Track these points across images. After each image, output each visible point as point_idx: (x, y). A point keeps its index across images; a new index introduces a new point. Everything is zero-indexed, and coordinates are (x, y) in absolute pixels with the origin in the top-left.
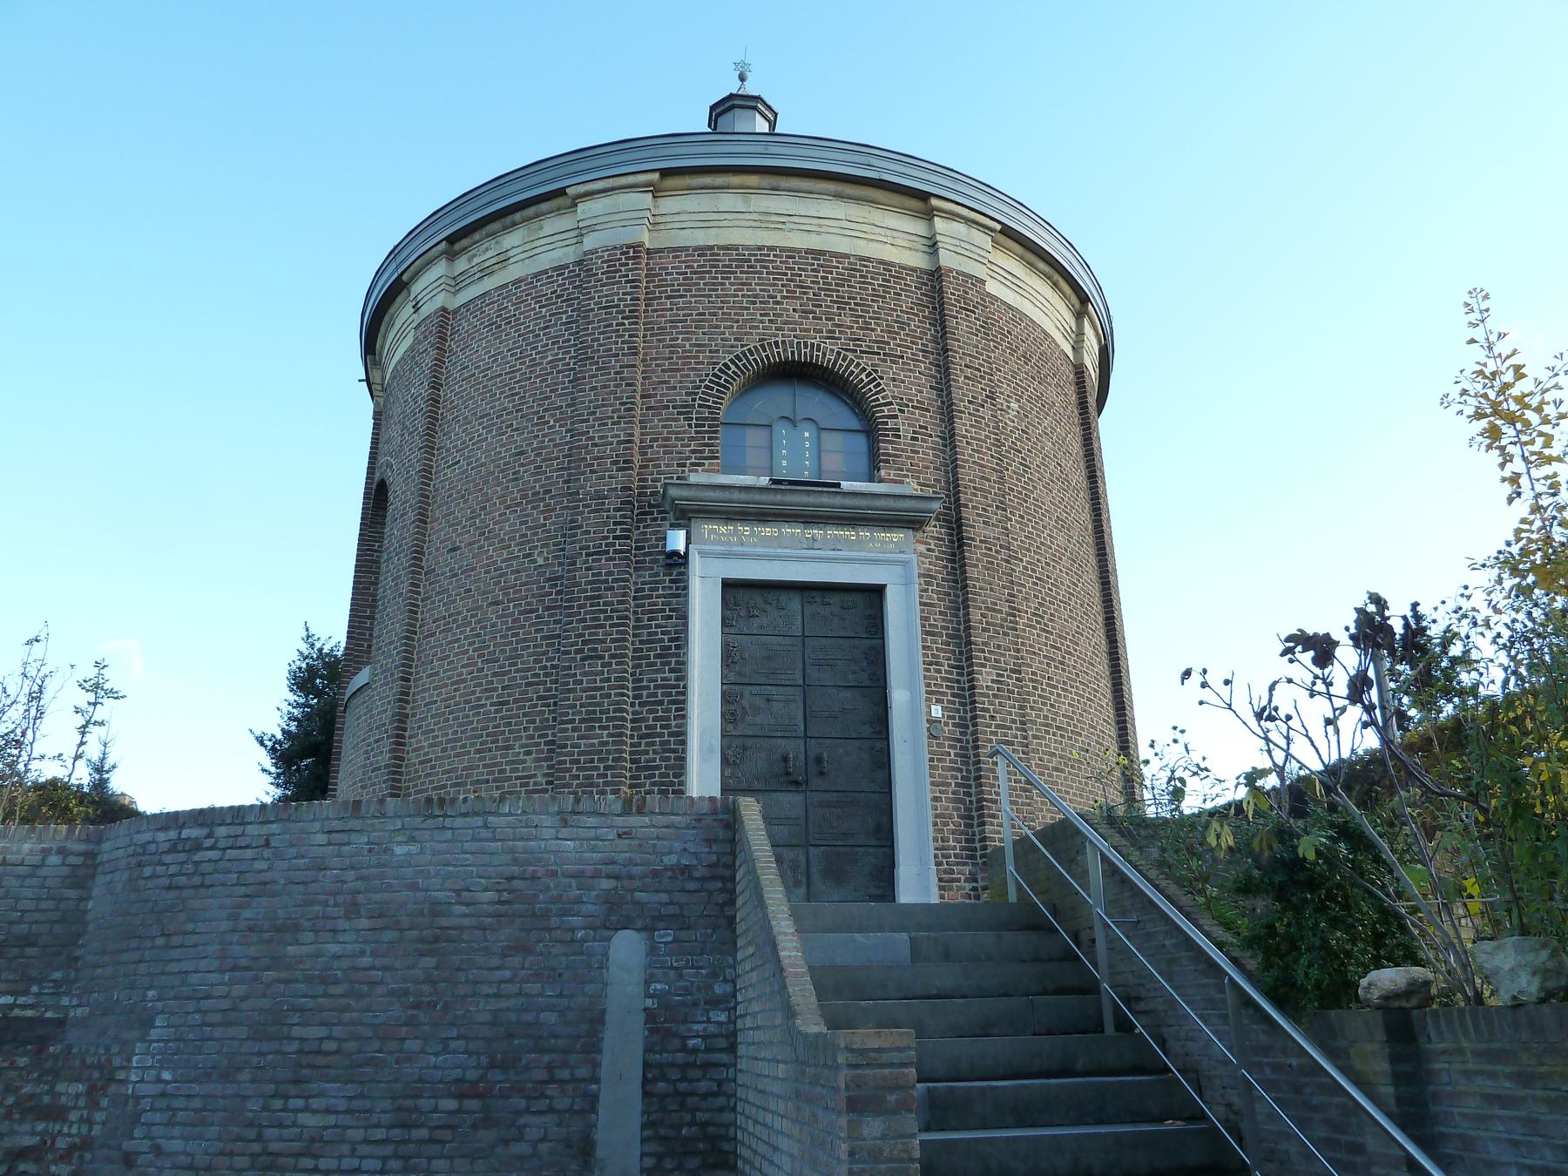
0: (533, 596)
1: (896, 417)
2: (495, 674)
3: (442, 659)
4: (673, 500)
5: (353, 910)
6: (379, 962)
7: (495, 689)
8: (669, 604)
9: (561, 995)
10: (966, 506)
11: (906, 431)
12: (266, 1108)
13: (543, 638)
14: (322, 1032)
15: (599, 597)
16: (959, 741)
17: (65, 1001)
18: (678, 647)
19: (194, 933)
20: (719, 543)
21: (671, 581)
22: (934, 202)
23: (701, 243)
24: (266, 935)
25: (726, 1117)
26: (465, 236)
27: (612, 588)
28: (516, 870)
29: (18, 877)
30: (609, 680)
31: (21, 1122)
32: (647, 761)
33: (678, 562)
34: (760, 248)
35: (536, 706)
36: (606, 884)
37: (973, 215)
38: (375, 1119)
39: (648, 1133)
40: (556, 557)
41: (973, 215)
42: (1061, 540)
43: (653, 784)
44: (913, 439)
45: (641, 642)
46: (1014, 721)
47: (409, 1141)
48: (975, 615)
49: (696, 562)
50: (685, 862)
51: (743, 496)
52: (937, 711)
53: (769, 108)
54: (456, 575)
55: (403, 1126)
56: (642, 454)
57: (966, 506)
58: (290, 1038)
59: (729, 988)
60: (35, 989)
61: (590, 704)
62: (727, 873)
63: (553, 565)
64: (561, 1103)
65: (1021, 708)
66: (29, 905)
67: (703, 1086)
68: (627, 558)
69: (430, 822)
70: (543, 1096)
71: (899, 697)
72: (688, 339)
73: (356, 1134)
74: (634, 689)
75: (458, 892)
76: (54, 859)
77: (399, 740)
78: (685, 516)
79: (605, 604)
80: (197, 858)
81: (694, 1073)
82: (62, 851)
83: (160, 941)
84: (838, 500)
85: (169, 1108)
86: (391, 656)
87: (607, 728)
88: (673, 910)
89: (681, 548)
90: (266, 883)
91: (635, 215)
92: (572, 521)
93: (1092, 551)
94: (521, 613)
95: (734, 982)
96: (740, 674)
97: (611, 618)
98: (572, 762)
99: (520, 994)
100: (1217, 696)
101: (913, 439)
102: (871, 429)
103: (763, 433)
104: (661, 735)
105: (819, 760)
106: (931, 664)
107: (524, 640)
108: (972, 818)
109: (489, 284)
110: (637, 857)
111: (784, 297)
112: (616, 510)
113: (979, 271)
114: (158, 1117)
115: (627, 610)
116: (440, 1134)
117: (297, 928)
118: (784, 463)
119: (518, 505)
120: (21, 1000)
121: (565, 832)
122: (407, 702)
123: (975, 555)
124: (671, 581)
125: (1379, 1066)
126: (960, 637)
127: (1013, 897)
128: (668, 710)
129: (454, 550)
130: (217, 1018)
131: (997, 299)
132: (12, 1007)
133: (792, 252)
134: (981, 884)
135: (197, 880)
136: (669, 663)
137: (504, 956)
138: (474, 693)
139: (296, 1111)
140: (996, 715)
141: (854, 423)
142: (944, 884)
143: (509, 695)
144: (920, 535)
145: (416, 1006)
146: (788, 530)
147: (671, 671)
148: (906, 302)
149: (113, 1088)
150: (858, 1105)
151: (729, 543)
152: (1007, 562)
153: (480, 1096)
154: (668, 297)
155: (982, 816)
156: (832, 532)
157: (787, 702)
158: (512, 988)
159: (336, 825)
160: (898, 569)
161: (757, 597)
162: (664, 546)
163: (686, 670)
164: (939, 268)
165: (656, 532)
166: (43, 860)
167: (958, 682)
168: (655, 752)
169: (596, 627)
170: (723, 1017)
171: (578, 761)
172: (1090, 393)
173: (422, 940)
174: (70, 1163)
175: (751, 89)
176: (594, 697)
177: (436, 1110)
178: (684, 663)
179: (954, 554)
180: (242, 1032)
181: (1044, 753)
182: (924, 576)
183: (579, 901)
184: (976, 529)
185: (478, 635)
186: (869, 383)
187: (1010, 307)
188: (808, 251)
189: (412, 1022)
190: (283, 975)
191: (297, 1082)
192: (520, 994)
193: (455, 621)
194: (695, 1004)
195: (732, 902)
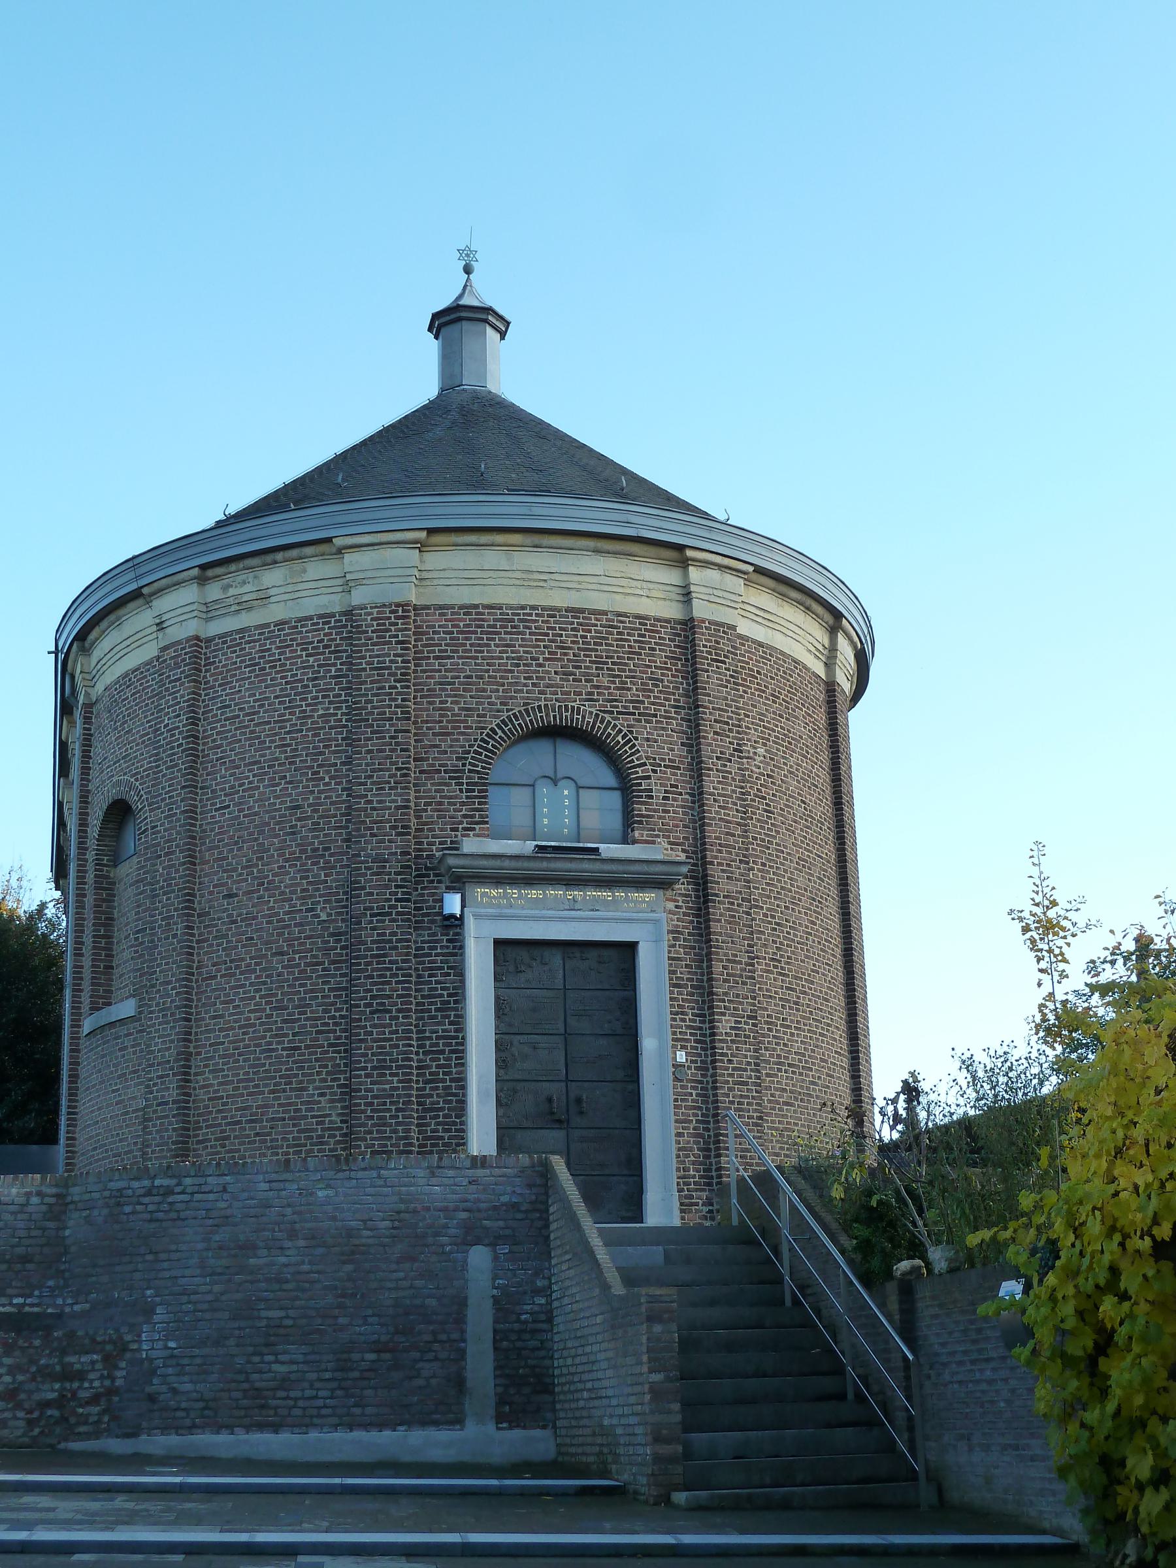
0: (319, 949)
1: (649, 777)
4: (451, 868)
5: (293, 1235)
6: (315, 1268)
7: (286, 1035)
9: (438, 1288)
10: (712, 863)
11: (658, 792)
12: (249, 1362)
14: (282, 1313)
16: (701, 1082)
17: (60, 1301)
18: (456, 1002)
19: (177, 1251)
20: (491, 906)
23: (467, 601)
24: (233, 1252)
25: (547, 1362)
27: (396, 948)
28: (403, 1206)
29: (12, 1213)
30: (397, 1032)
31: (43, 1383)
32: (432, 1103)
33: (454, 924)
34: (523, 608)
35: (327, 1052)
36: (464, 1215)
37: (727, 561)
38: (323, 1366)
39: (498, 1372)
41: (727, 561)
42: (801, 881)
43: (438, 1124)
44: (665, 798)
45: (423, 997)
46: (749, 1063)
47: (348, 1379)
48: (717, 967)
49: (471, 925)
50: (514, 1200)
51: (514, 864)
52: (681, 1057)
53: (501, 318)
55: (342, 1370)
56: (419, 817)
57: (712, 863)
58: (260, 1318)
59: (546, 1282)
60: (36, 1293)
61: (381, 1054)
62: (542, 1207)
63: (336, 921)
64: (443, 1355)
65: (756, 1051)
66: (22, 1233)
67: (532, 1343)
68: (409, 920)
69: (340, 1175)
70: (430, 1350)
71: (649, 1044)
72: (457, 703)
73: (314, 1376)
74: (418, 1039)
75: (364, 1221)
76: (35, 1200)
77: (185, 1077)
78: (459, 882)
79: (390, 962)
80: (170, 1199)
81: (527, 1336)
82: (39, 1194)
83: (149, 1257)
84: (598, 866)
85: (178, 1365)
86: (169, 996)
87: (397, 1075)
88: (508, 1232)
89: (458, 912)
90: (227, 1217)
93: (834, 883)
95: (550, 1279)
96: (510, 1025)
97: (396, 975)
98: (366, 1104)
99: (411, 1287)
100: (947, 1015)
101: (665, 798)
102: (627, 788)
103: (527, 791)
104: (443, 1081)
105: (579, 1101)
106: (677, 1013)
107: (312, 991)
108: (709, 1150)
110: (482, 1197)
111: (545, 659)
114: (170, 1371)
115: (410, 968)
116: (367, 1374)
117: (254, 1247)
118: (546, 821)
120: (29, 1301)
121: (434, 1181)
122: (190, 1041)
123: (719, 910)
125: (894, 1305)
126: (702, 987)
127: (735, 1222)
128: (450, 1059)
129: (230, 896)
130: (205, 1306)
132: (24, 1305)
133: (553, 611)
134: (716, 1207)
135: (173, 1215)
136: (448, 1017)
137: (398, 1263)
138: (264, 1037)
139: (269, 1363)
140: (734, 1057)
141: (610, 780)
142: (685, 1207)
143: (301, 1041)
144: (669, 893)
145: (343, 1296)
148: (660, 657)
149: (128, 1355)
150: (651, 1319)
151: (499, 906)
152: (748, 914)
153: (389, 1351)
155: (718, 1149)
156: (592, 893)
158: (405, 1284)
159: (274, 1176)
160: (650, 927)
161: (523, 954)
162: (442, 907)
163: (464, 1023)
164: (692, 619)
165: (433, 894)
166: (28, 1200)
167: (700, 1029)
170: (543, 1301)
171: (372, 1104)
172: (834, 707)
173: (342, 1254)
174: (99, 1405)
176: (384, 1047)
177: (363, 1360)
178: (461, 1016)
179: (699, 909)
180: (226, 1315)
181: (776, 1089)
183: (446, 1227)
184: (721, 885)
185: (265, 983)
186: (625, 744)
187: (761, 644)
189: (340, 1306)
190: (249, 1278)
191: (267, 1345)
192: (411, 1287)
193: (237, 967)
194: (525, 1293)
195: (547, 1226)
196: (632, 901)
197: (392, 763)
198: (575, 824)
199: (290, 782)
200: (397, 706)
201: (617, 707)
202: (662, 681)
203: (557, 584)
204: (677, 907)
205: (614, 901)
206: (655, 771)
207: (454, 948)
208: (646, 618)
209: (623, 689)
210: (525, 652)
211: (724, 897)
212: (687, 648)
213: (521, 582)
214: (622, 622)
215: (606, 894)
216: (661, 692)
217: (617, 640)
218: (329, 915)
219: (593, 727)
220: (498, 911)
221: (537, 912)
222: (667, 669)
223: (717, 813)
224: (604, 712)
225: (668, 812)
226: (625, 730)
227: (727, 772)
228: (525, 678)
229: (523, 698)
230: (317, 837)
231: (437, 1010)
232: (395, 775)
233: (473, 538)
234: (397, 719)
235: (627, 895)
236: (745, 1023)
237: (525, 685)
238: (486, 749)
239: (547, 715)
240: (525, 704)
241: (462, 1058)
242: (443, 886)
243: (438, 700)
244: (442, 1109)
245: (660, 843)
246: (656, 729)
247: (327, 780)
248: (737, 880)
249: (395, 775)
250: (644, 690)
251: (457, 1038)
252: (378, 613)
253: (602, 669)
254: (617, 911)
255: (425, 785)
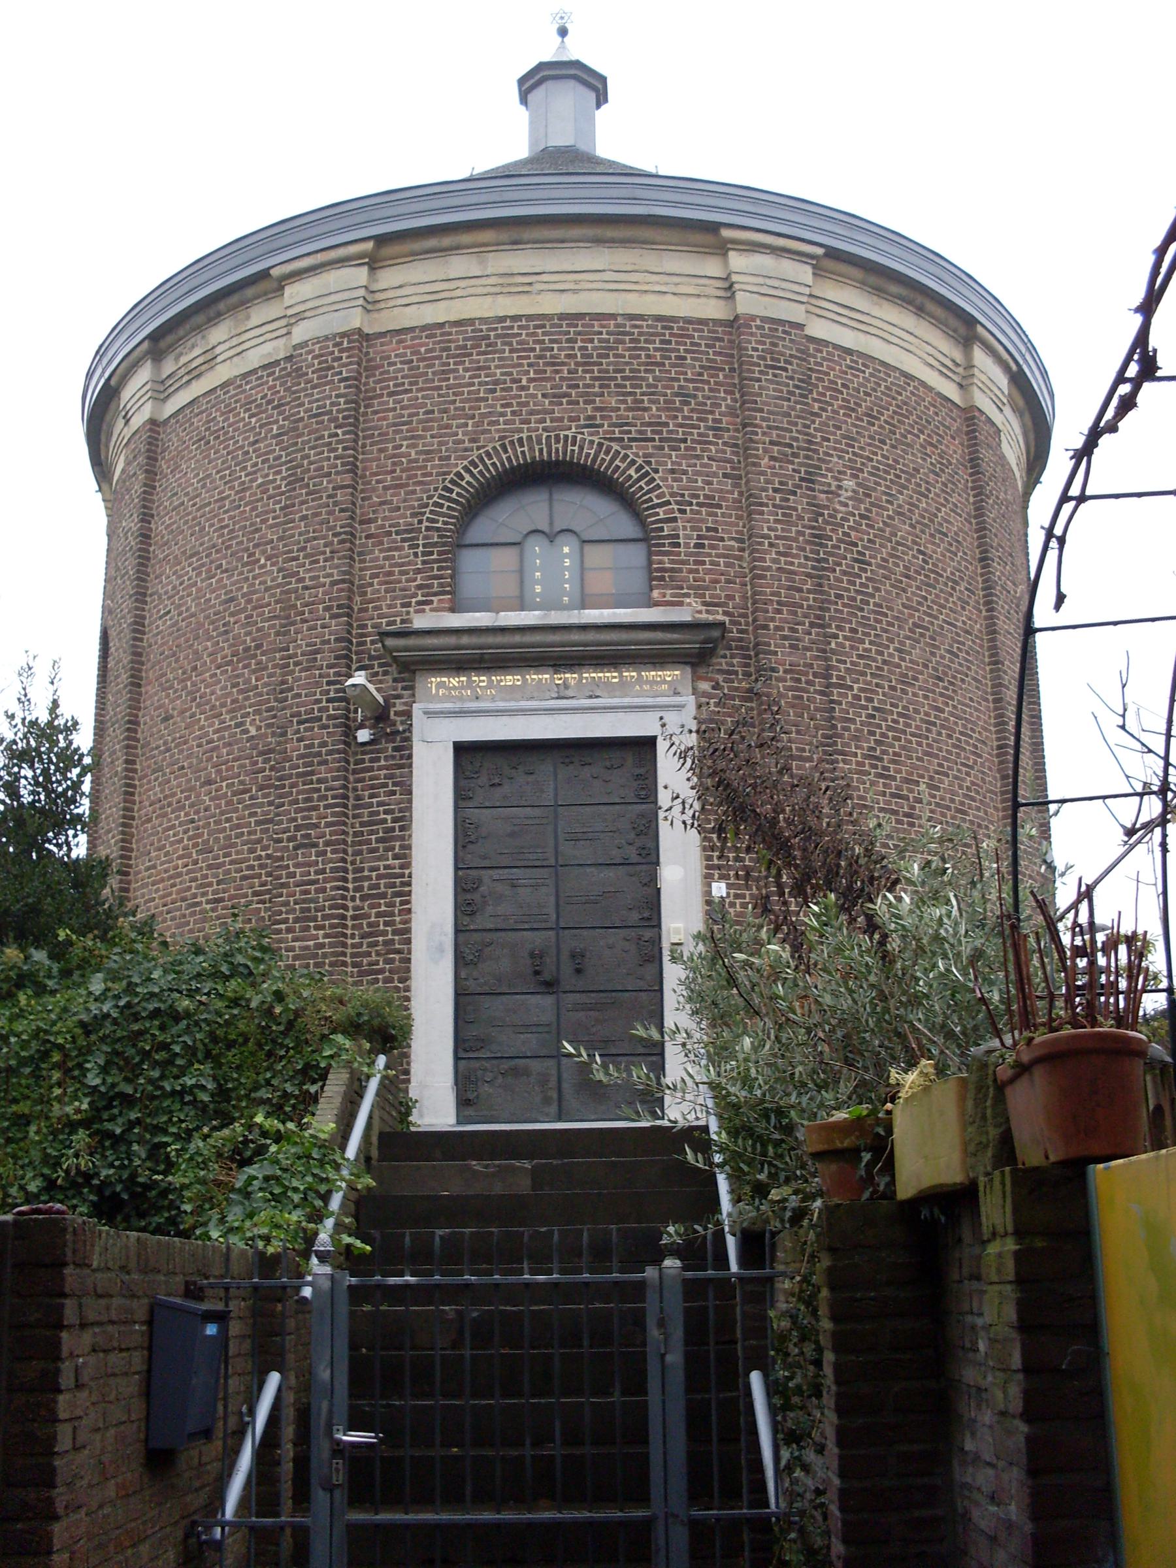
1: (675, 520)
2: (210, 867)
7: (210, 885)
13: (258, 823)
18: (402, 829)
20: (449, 698)
21: (395, 749)
22: (726, 233)
23: (430, 320)
30: (323, 871)
32: (370, 964)
34: (502, 319)
37: (782, 242)
40: (268, 726)
41: (782, 242)
45: (362, 824)
54: (168, 750)
61: (304, 901)
72: (414, 446)
79: (319, 781)
87: (322, 927)
91: (346, 295)
92: (283, 682)
94: (234, 794)
97: (325, 798)
101: (697, 546)
103: (512, 552)
104: (385, 933)
107: (238, 826)
111: (530, 380)
112: (330, 667)
113: (796, 313)
118: (538, 589)
119: (230, 663)
129: (166, 719)
131: (826, 343)
141: (625, 526)
147: (396, 857)
151: (461, 698)
154: (391, 394)
156: (589, 675)
157: (535, 886)
168: (378, 954)
175: (577, 50)
178: (409, 847)
185: (192, 821)
187: (849, 351)
188: (562, 317)
193: (170, 805)
196: (647, 682)
199: (226, 571)
200: (336, 458)
202: (695, 397)
203: (545, 287)
205: (623, 683)
206: (683, 512)
207: (402, 757)
209: (639, 409)
210: (502, 374)
211: (786, 671)
212: (732, 356)
213: (497, 289)
214: (636, 326)
215: (611, 676)
217: (630, 349)
218: (259, 728)
219: (594, 460)
222: (702, 381)
223: (774, 561)
224: (611, 440)
225: (704, 563)
226: (640, 461)
227: (789, 508)
228: (503, 406)
229: (498, 431)
231: (378, 841)
232: (332, 543)
233: (432, 243)
235: (639, 675)
237: (503, 415)
239: (531, 449)
240: (501, 438)
244: (382, 971)
245: (689, 604)
249: (332, 543)
251: (403, 875)
252: (321, 349)
253: (608, 386)
255: (372, 552)
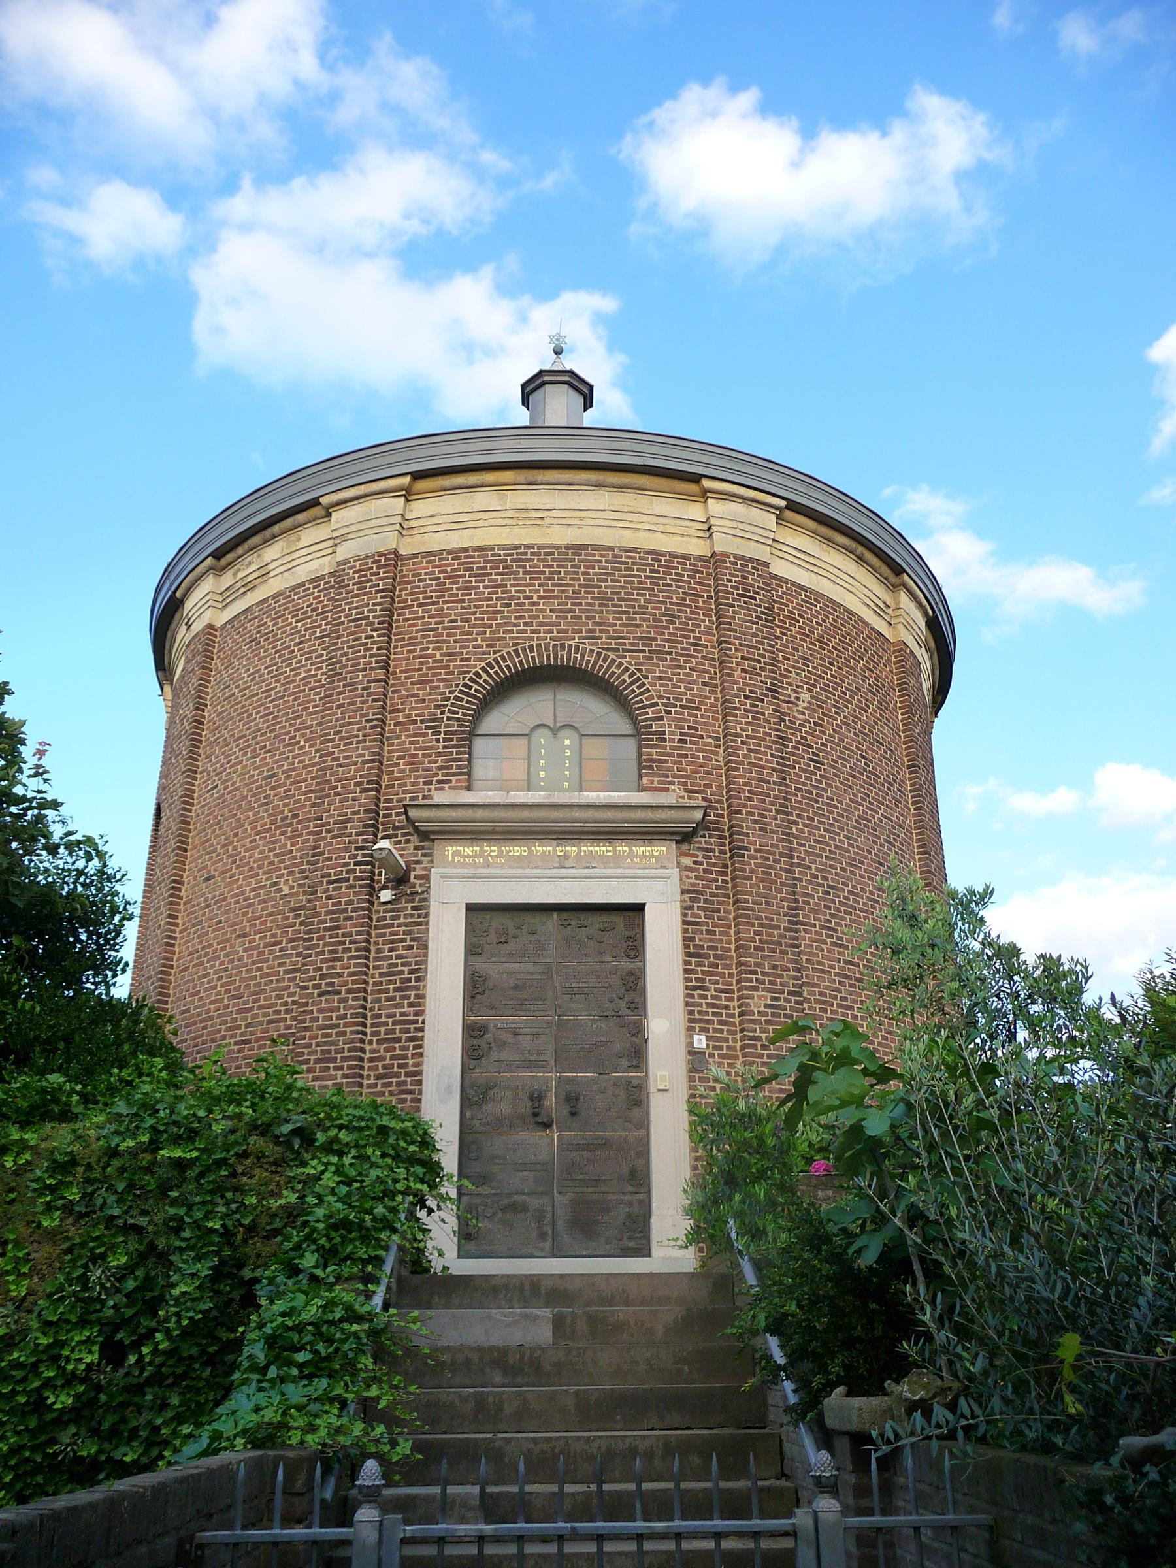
0: (278, 927)
1: (661, 719)
2: (240, 1011)
3: (194, 995)
7: (239, 1027)
8: (410, 932)
15: (337, 928)
18: (418, 979)
20: (463, 865)
21: (414, 908)
22: (706, 483)
26: (229, 552)
27: (351, 918)
30: (344, 1017)
34: (518, 547)
40: (300, 886)
44: (680, 741)
54: (208, 906)
61: (326, 1043)
87: (341, 1068)
92: (315, 847)
94: (266, 945)
97: (349, 950)
101: (680, 741)
103: (523, 741)
106: (695, 988)
107: (268, 975)
109: (252, 599)
111: (540, 597)
112: (358, 834)
124: (414, 908)
129: (208, 879)
131: (786, 581)
133: (550, 549)
141: (626, 727)
143: (252, 1033)
146: (538, 848)
147: (411, 1005)
151: (474, 866)
154: (420, 605)
156: (587, 848)
161: (507, 921)
169: (334, 960)
178: (423, 996)
182: (688, 892)
186: (632, 684)
188: (568, 547)
193: (207, 954)
197: (363, 716)
198: (577, 777)
201: (624, 644)
204: (695, 863)
206: (669, 712)
207: (419, 916)
208: (662, 553)
210: (516, 592)
214: (631, 558)
215: (605, 849)
216: (676, 628)
217: (625, 576)
218: (292, 888)
220: (472, 871)
221: (520, 871)
222: (685, 605)
224: (608, 649)
226: (632, 668)
229: (512, 638)
230: (288, 805)
234: (371, 669)
236: (786, 1000)
238: (468, 695)
239: (540, 655)
241: (421, 1047)
242: (411, 846)
243: (418, 648)
246: (669, 667)
247: (302, 743)
248: (773, 832)
249: (365, 728)
250: (656, 627)
251: (416, 1022)
254: (619, 867)
255: (399, 737)
